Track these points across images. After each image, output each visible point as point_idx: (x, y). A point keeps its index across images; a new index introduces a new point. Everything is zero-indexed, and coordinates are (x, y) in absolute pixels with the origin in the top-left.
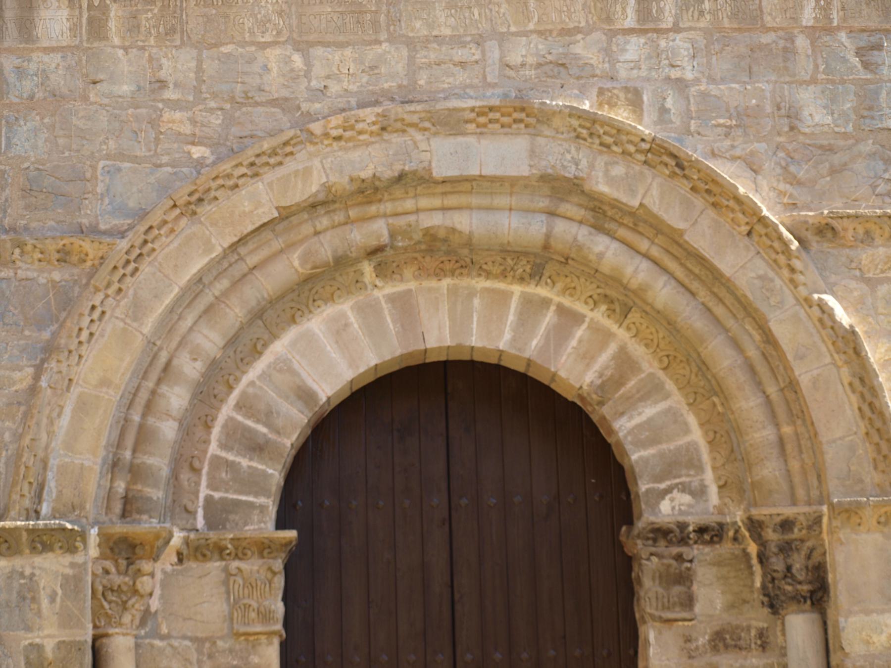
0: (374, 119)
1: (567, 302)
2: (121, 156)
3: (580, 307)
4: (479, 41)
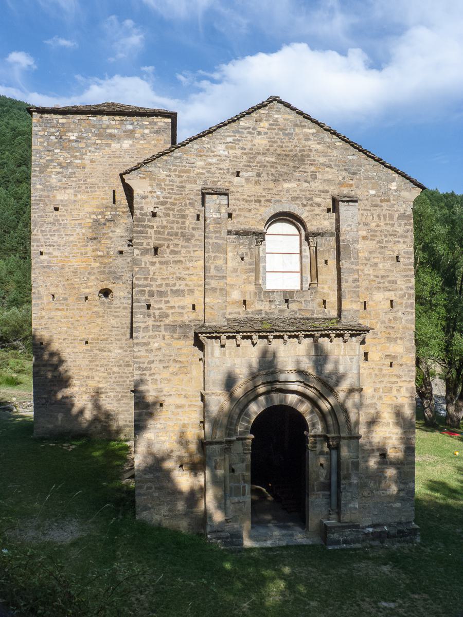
0: (152, 365)
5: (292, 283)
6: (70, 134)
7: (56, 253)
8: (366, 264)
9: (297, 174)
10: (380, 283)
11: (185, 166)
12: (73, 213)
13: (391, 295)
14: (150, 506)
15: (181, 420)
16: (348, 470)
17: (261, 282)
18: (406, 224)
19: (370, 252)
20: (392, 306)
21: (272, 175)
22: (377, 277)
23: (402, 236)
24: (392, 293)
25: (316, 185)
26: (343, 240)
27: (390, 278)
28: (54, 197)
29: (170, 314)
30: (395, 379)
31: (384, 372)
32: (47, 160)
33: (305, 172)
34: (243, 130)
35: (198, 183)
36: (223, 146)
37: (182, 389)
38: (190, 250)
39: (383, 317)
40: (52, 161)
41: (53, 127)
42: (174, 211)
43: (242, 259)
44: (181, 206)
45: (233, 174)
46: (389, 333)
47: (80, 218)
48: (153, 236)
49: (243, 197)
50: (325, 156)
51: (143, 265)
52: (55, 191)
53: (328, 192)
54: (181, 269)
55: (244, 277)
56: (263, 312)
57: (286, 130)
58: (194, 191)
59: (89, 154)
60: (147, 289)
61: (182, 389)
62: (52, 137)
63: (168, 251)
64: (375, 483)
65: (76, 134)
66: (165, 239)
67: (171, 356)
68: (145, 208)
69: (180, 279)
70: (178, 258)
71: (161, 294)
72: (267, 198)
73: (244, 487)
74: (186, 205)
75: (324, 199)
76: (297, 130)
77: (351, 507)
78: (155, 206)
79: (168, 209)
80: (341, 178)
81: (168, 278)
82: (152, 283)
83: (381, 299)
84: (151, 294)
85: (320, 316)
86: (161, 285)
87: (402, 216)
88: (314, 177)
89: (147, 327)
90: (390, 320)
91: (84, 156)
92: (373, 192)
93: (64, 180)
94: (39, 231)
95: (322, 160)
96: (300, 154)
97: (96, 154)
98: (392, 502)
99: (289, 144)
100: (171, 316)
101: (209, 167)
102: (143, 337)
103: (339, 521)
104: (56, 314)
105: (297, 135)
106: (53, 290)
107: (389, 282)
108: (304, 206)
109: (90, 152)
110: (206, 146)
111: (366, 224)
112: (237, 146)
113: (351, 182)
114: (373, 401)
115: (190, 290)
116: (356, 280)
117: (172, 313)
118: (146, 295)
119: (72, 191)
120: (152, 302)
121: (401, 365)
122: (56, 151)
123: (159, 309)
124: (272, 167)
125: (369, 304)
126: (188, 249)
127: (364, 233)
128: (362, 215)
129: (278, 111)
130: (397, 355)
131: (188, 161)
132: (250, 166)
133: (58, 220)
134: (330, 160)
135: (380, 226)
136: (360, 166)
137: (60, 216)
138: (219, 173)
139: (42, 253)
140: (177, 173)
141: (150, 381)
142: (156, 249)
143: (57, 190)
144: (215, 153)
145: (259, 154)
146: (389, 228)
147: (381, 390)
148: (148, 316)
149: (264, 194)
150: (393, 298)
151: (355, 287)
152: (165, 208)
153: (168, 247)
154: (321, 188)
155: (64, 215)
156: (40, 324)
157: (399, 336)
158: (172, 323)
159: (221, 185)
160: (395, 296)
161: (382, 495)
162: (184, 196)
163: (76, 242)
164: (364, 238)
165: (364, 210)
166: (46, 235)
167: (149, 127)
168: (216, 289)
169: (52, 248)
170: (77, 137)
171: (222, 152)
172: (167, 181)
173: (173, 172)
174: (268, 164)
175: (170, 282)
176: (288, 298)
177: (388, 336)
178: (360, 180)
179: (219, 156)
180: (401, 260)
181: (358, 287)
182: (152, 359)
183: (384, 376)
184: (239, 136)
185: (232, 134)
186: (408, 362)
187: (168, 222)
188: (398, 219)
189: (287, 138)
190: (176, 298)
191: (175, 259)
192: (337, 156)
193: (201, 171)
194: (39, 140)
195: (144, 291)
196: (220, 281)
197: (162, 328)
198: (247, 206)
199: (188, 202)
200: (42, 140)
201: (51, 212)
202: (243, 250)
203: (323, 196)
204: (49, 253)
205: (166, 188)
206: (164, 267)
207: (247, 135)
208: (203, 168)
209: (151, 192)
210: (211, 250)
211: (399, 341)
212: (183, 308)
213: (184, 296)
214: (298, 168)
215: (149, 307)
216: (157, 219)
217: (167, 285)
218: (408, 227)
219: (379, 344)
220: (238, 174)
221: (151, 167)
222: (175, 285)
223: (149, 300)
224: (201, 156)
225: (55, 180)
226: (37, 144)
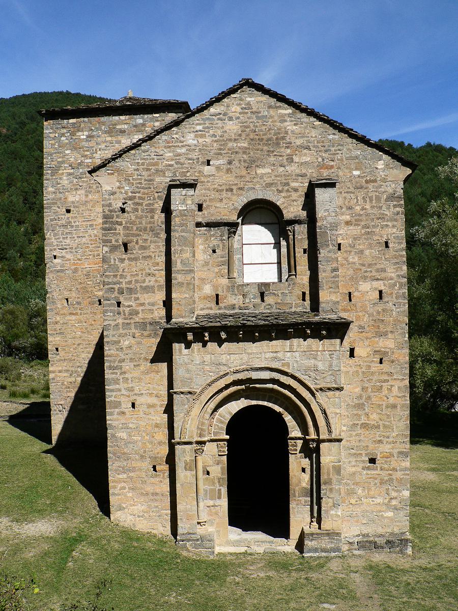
0: (123, 364)
1: (276, 396)
2: (198, 375)
3: (279, 398)
4: (261, 353)
5: (269, 275)
6: (80, 133)
7: (68, 256)
8: (350, 252)
9: (272, 159)
10: (366, 272)
11: (153, 159)
12: (85, 214)
13: (380, 285)
14: (124, 506)
15: (153, 420)
16: (329, 474)
17: (235, 275)
18: (395, 206)
19: (355, 239)
20: (381, 298)
21: (245, 161)
22: (363, 265)
23: (391, 220)
24: (381, 282)
25: (292, 169)
26: (320, 227)
27: (378, 266)
28: (66, 198)
29: (140, 311)
30: (386, 377)
31: (373, 369)
32: (59, 162)
33: (281, 156)
34: (214, 117)
35: (167, 175)
36: (192, 135)
37: (153, 388)
38: (159, 244)
39: (370, 309)
40: (63, 162)
41: (64, 128)
42: (142, 205)
43: (214, 251)
44: (150, 199)
45: (203, 163)
46: (379, 326)
47: (92, 218)
48: (122, 232)
49: (213, 187)
50: (302, 137)
51: (112, 262)
52: (67, 193)
53: (306, 175)
54: (151, 264)
55: (216, 270)
56: (237, 306)
57: (260, 112)
58: (163, 183)
59: (99, 152)
60: (116, 287)
61: (153, 388)
62: (63, 138)
63: (137, 247)
64: (364, 490)
65: (86, 133)
66: (133, 235)
67: (141, 354)
68: (113, 204)
69: (149, 275)
70: (147, 253)
71: (131, 291)
72: (239, 186)
73: (220, 490)
74: (154, 199)
75: (302, 183)
76: (272, 112)
77: (332, 514)
78: (124, 201)
79: (138, 204)
80: (320, 160)
81: (137, 275)
82: (121, 280)
83: (369, 289)
84: (121, 292)
85: (298, 310)
86: (130, 282)
87: (392, 197)
88: (290, 160)
89: (117, 325)
90: (378, 313)
91: (94, 155)
92: (356, 173)
93: (75, 181)
94: (52, 234)
95: (299, 142)
96: (275, 137)
97: (106, 152)
98: (383, 511)
99: (263, 128)
100: (141, 313)
101: (178, 158)
102: (113, 336)
103: (320, 528)
104: (71, 318)
105: (272, 117)
106: (66, 294)
107: (377, 271)
108: (280, 192)
109: (100, 150)
110: (174, 136)
111: (350, 208)
112: (207, 134)
113: (332, 163)
114: (361, 402)
115: (161, 285)
116: (335, 270)
117: (142, 310)
118: (116, 292)
119: (83, 192)
120: (121, 300)
121: (393, 362)
122: (67, 152)
123: (129, 306)
124: (244, 153)
125: (355, 294)
126: (157, 244)
127: (348, 218)
128: (345, 198)
129: (251, 95)
130: (388, 350)
131: (156, 154)
132: (221, 154)
133: (70, 222)
134: (308, 141)
135: (366, 209)
136: (342, 145)
137: (72, 217)
138: (189, 163)
139: (55, 257)
140: (145, 167)
141: (121, 380)
142: (125, 245)
143: (68, 191)
144: (184, 143)
145: (230, 140)
146: (375, 211)
147: (370, 390)
148: (118, 313)
149: (236, 182)
150: (382, 288)
151: (333, 277)
152: (133, 204)
153: (137, 243)
154: (298, 171)
155: (76, 217)
156: (55, 330)
157: (389, 329)
158: (142, 321)
159: (189, 178)
160: (384, 285)
161: (372, 503)
162: (152, 189)
163: (88, 244)
164: (348, 223)
165: (347, 192)
166: (58, 239)
167: (160, 119)
168: (183, 284)
169: (65, 251)
170: (88, 136)
171: (191, 142)
172: (136, 175)
173: (142, 165)
174: (240, 151)
175: (139, 278)
176: (263, 290)
177: (377, 330)
178: (342, 160)
179: (188, 146)
180: (391, 245)
181: (338, 276)
182: (123, 357)
183: (373, 374)
184: (209, 124)
185: (202, 122)
186: (400, 358)
187: (137, 217)
188: (386, 201)
189: (260, 121)
190: (146, 296)
191: (144, 255)
192: (316, 137)
193: (170, 163)
194: (50, 142)
195: (114, 288)
196: (187, 275)
197: (133, 326)
198: (217, 195)
199: (156, 195)
200: (53, 142)
201: (62, 215)
202: (214, 242)
203: (300, 180)
204: (62, 257)
205: (134, 182)
206: (133, 263)
207: (217, 122)
208: (172, 160)
209: (119, 188)
210: (177, 244)
211: (390, 335)
212: (153, 304)
213: (154, 292)
214: (273, 152)
215: (119, 304)
216: (125, 214)
217: (137, 281)
218: (398, 209)
219: (367, 338)
220: (208, 163)
221: (119, 163)
222: (144, 281)
223: (119, 297)
224: (169, 147)
225: (66, 182)
226: (47, 145)
